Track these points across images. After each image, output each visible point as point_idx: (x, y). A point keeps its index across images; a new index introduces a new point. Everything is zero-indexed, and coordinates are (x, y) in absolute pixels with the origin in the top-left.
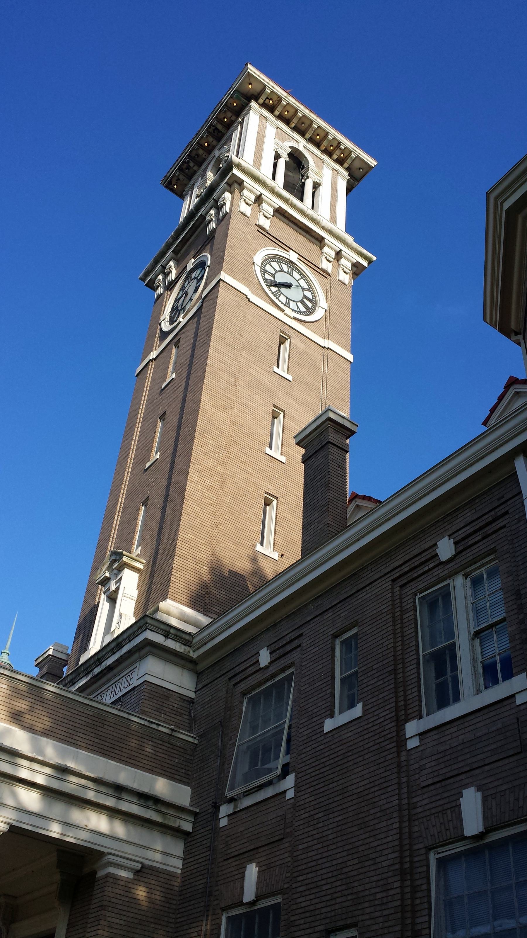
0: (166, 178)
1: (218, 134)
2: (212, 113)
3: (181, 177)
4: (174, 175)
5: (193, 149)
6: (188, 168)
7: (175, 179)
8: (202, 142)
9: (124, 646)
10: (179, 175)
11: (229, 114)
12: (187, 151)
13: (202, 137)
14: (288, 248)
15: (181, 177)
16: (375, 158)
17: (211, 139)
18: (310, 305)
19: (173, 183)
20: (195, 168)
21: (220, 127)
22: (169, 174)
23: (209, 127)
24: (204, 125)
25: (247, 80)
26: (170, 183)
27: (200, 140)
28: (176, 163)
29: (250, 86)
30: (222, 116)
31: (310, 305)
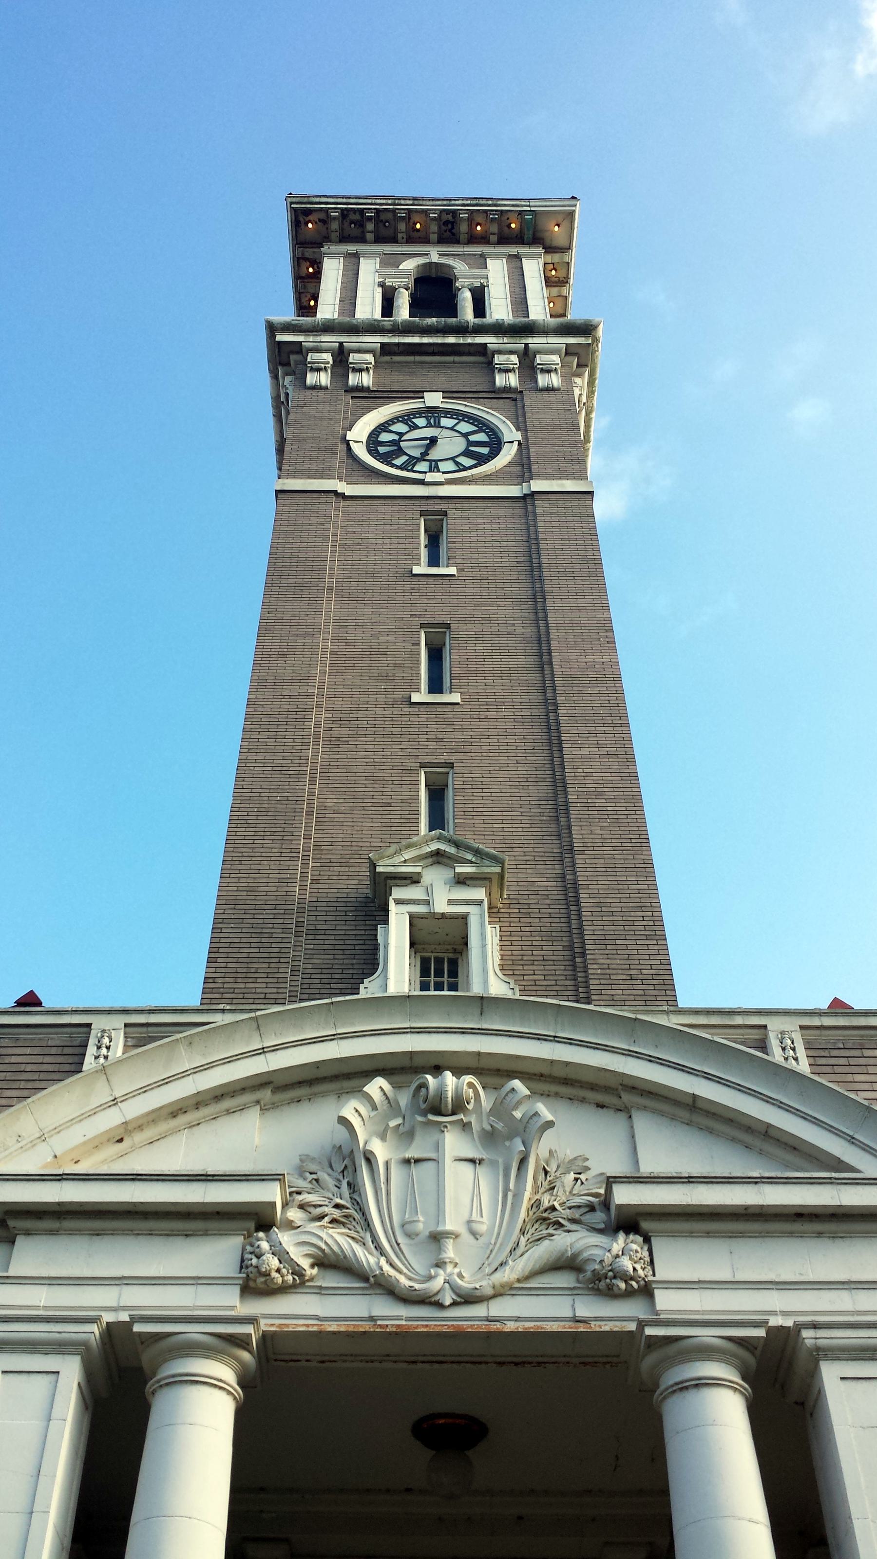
0: (306, 200)
1: (445, 231)
2: (467, 199)
3: (335, 226)
4: (327, 211)
5: (394, 211)
6: (361, 224)
7: (322, 216)
8: (415, 217)
9: (275, 377)
10: (335, 218)
11: (494, 228)
12: (378, 201)
13: (426, 212)
14: (418, 394)
15: (335, 226)
16: (140, 1334)
17: (434, 228)
18: (382, 450)
19: (310, 218)
20: (370, 236)
21: (464, 228)
22: (317, 200)
23: (448, 212)
24: (438, 200)
25: (560, 219)
26: (307, 212)
27: (416, 211)
28: (343, 197)
29: (556, 228)
30: (480, 218)
31: (382, 450)
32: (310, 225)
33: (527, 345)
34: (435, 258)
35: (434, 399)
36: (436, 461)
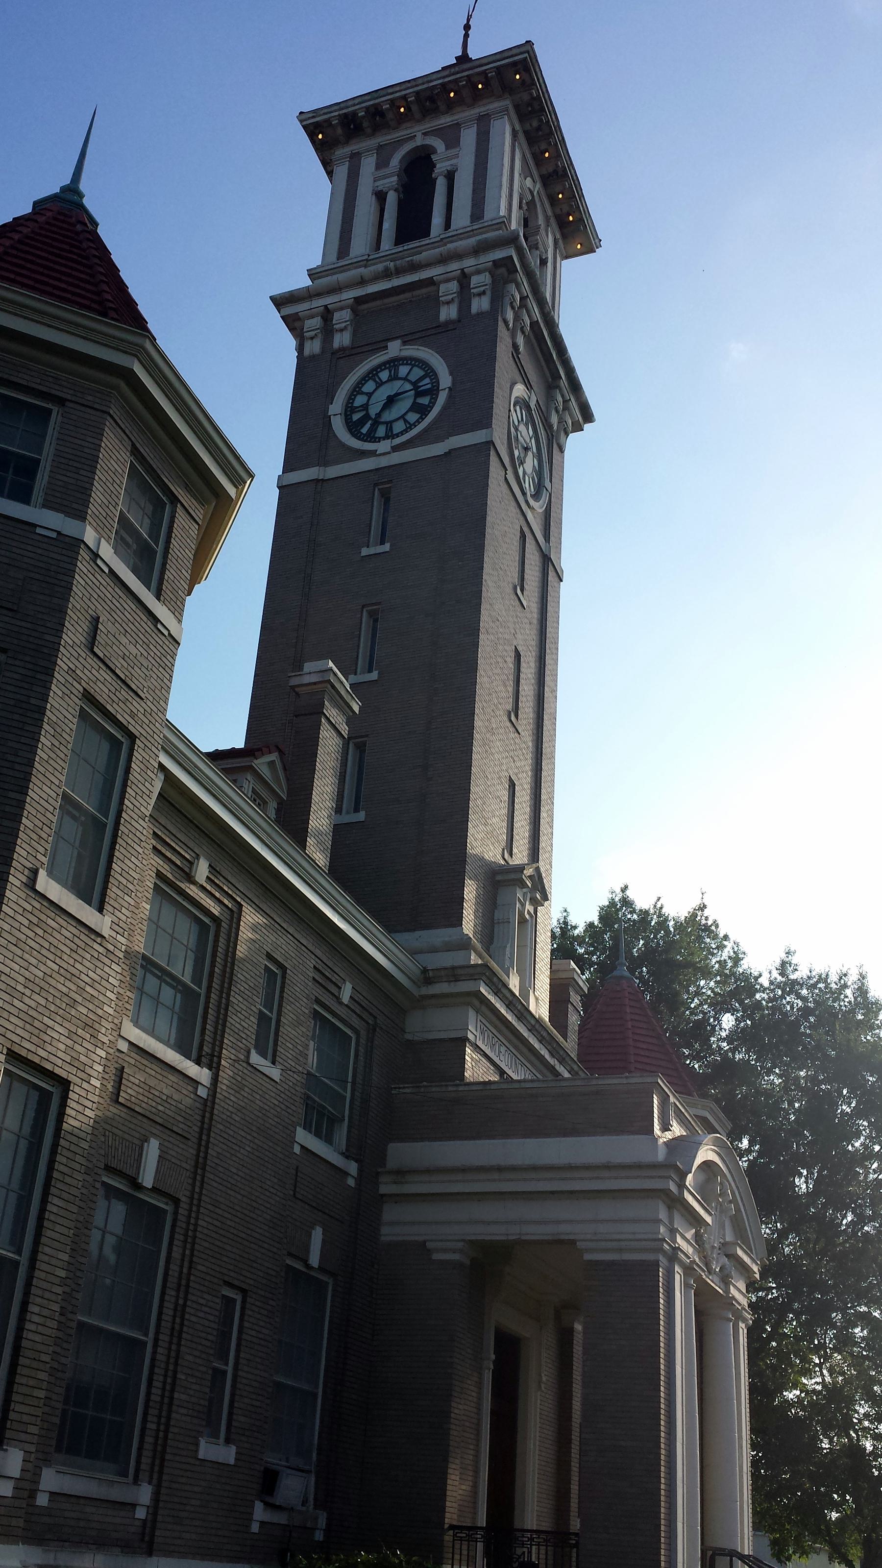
32: (518, 77)
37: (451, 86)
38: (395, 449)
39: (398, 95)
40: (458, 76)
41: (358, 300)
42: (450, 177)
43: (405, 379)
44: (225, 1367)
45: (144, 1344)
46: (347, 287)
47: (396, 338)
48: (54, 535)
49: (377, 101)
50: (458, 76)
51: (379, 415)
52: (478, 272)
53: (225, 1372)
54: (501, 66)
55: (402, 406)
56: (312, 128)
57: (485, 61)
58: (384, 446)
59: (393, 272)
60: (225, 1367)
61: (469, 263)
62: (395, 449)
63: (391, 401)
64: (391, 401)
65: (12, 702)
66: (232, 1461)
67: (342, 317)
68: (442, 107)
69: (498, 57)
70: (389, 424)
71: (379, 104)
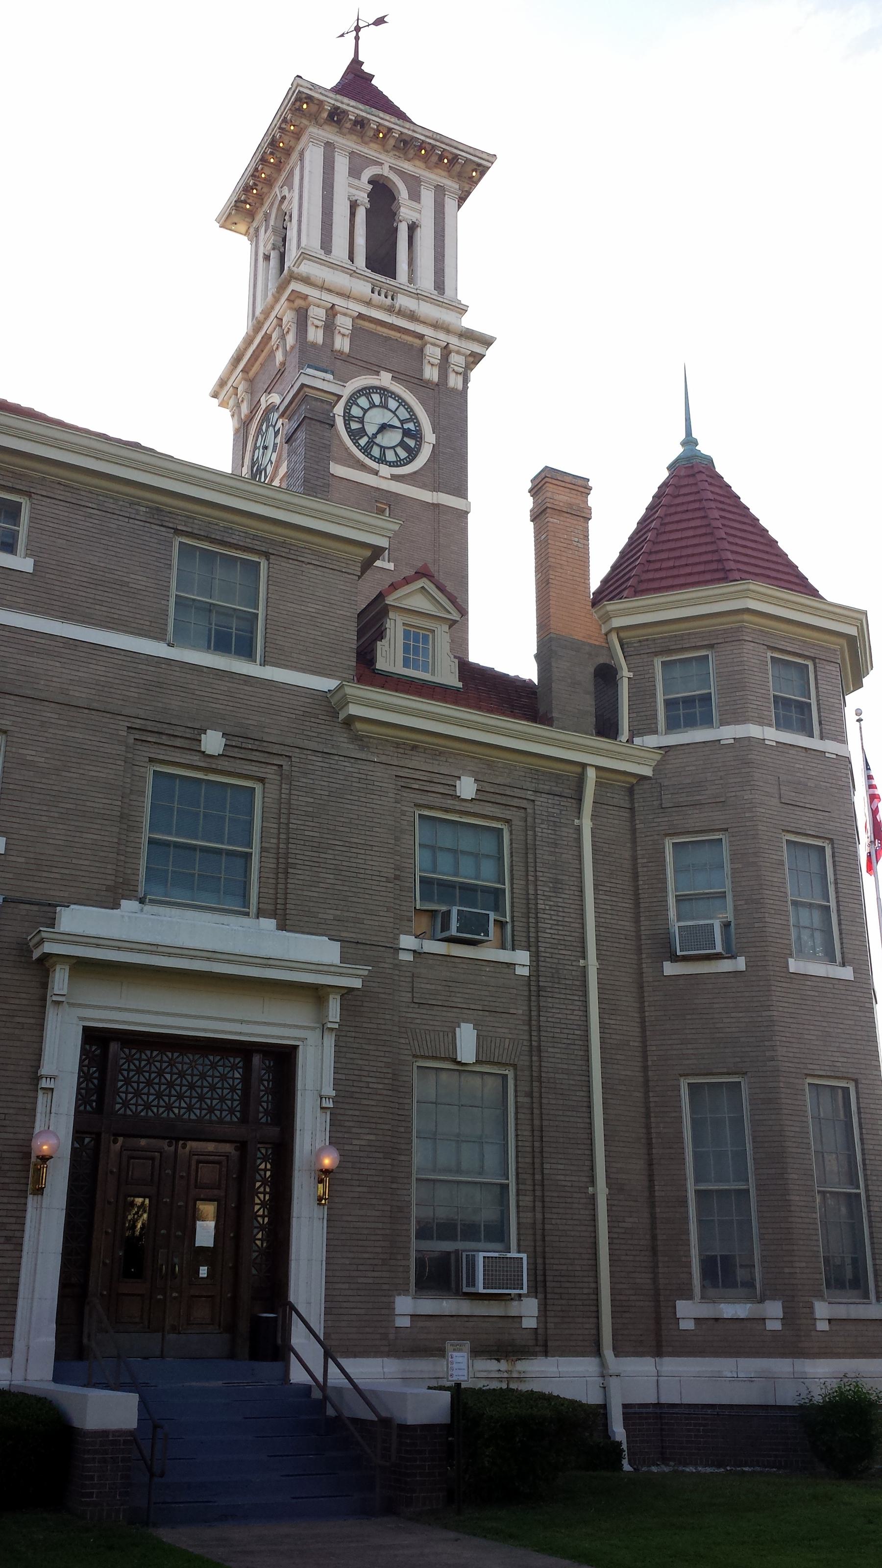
33: (334, 305)
34: (386, 171)
35: (385, 379)
36: (385, 448)
37: (427, 146)
38: (394, 478)
39: (387, 124)
40: (438, 144)
41: (361, 316)
42: (412, 228)
43: (365, 411)
44: (858, 1191)
45: (859, 1195)
46: (337, 293)
47: (390, 371)
48: (834, 756)
49: (369, 116)
50: (438, 144)
51: (375, 435)
52: (458, 353)
53: (859, 1195)
54: (471, 160)
55: (392, 438)
56: (304, 96)
57: (461, 147)
58: (385, 471)
59: (397, 309)
60: (858, 1191)
61: (454, 341)
62: (394, 478)
63: (383, 428)
64: (383, 428)
65: (301, 713)
66: (201, 1276)
67: (344, 323)
68: (411, 153)
69: (472, 151)
70: (383, 449)
71: (369, 120)
